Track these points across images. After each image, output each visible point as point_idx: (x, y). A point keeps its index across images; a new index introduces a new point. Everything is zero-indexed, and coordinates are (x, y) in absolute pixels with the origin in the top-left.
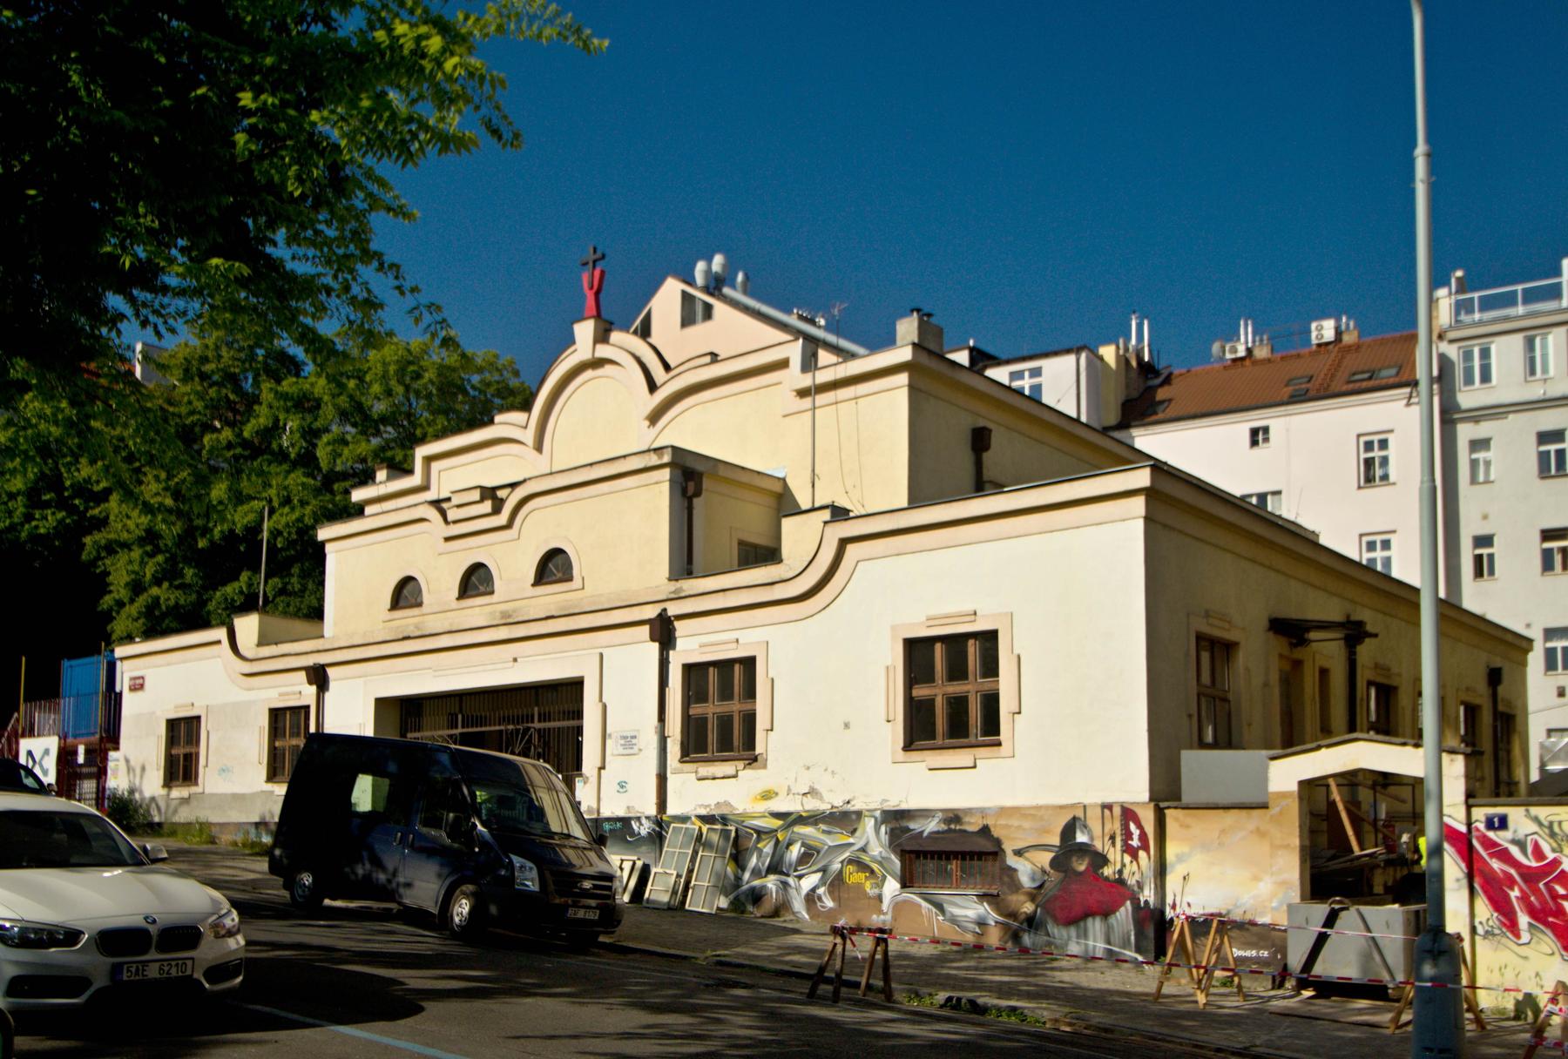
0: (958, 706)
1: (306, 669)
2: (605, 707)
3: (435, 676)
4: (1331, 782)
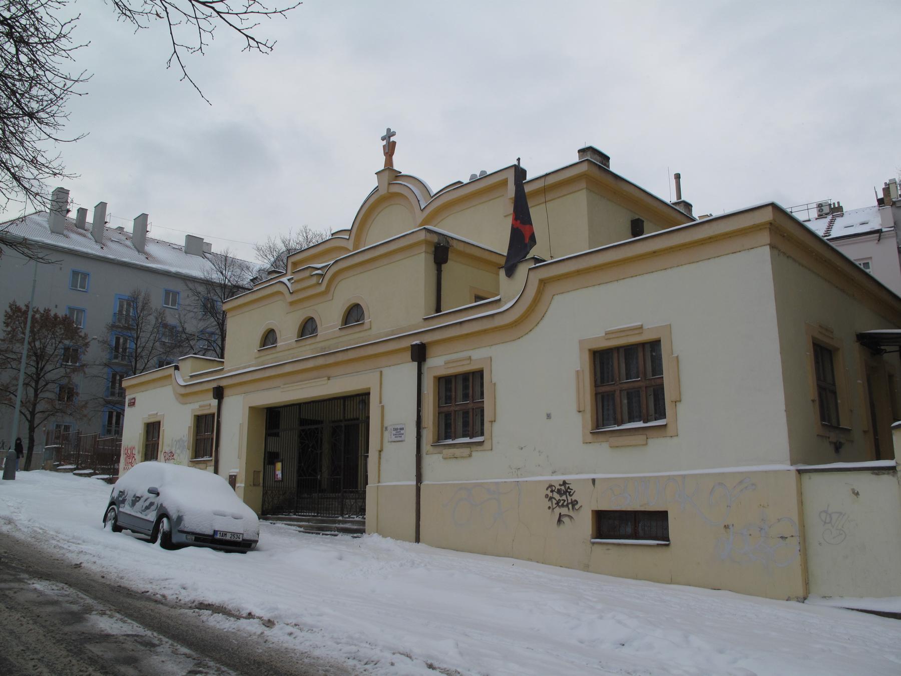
2: (383, 407)
3: (282, 392)
4: (198, 437)
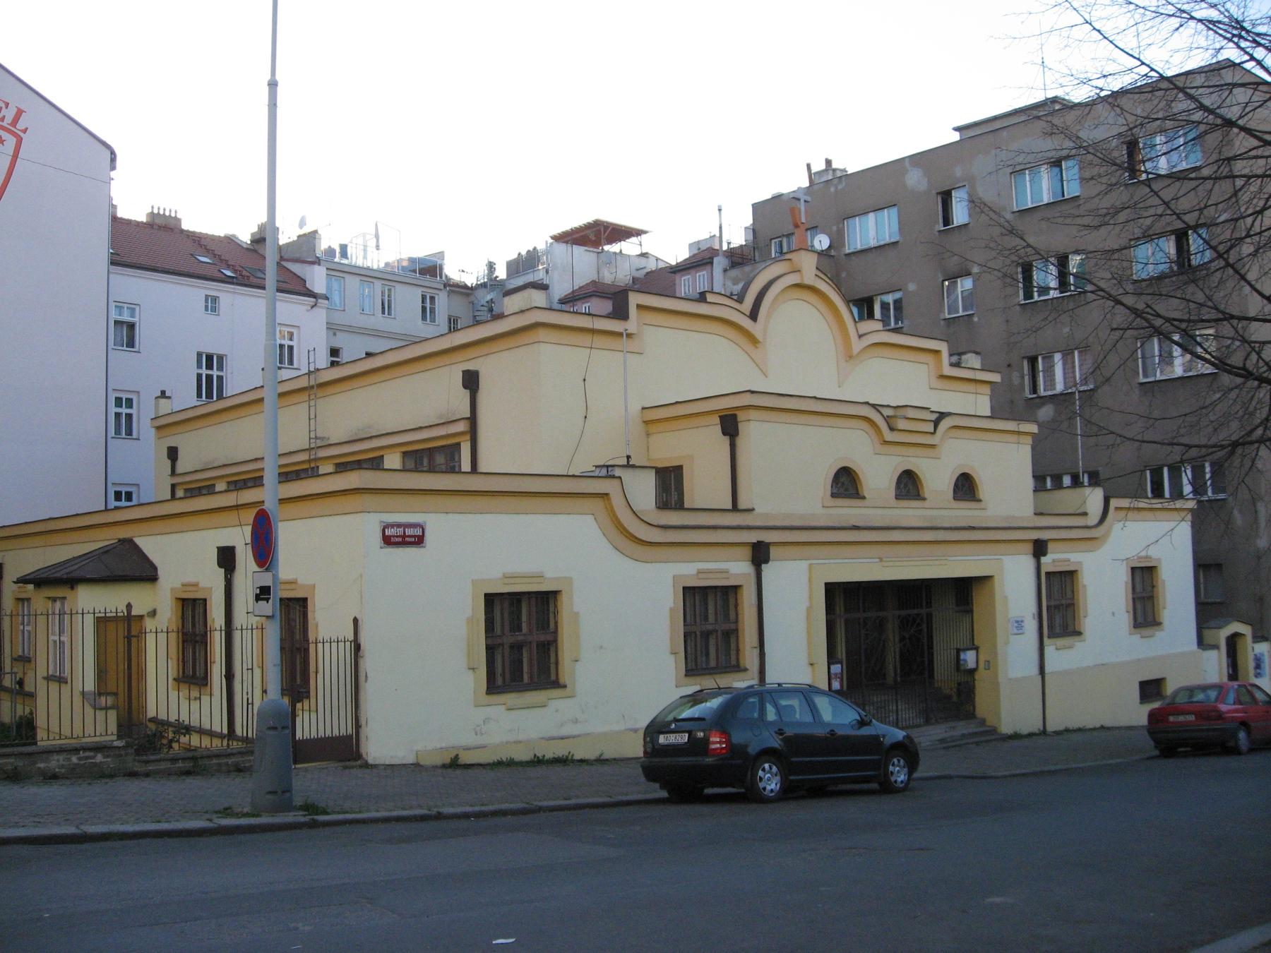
0: (210, 366)
1: (15, 127)
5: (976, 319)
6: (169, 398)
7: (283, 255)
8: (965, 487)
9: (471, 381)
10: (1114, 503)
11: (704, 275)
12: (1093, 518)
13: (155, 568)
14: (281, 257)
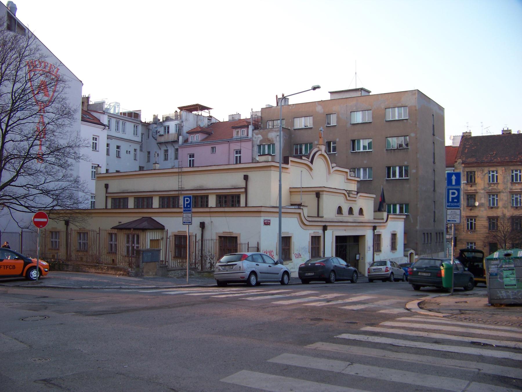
5: (337, 155)
6: (101, 167)
7: (88, 108)
8: (361, 212)
9: (246, 178)
10: (390, 216)
11: (244, 130)
12: (385, 221)
13: (164, 226)
14: (88, 109)
